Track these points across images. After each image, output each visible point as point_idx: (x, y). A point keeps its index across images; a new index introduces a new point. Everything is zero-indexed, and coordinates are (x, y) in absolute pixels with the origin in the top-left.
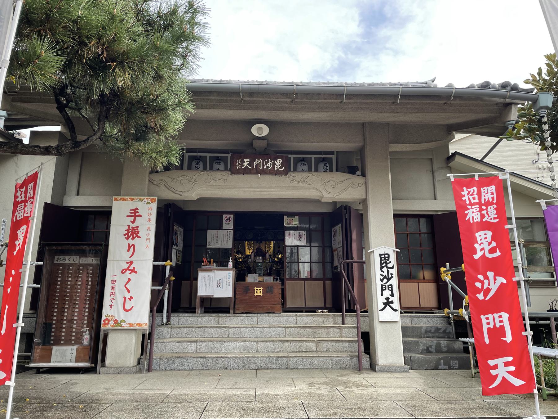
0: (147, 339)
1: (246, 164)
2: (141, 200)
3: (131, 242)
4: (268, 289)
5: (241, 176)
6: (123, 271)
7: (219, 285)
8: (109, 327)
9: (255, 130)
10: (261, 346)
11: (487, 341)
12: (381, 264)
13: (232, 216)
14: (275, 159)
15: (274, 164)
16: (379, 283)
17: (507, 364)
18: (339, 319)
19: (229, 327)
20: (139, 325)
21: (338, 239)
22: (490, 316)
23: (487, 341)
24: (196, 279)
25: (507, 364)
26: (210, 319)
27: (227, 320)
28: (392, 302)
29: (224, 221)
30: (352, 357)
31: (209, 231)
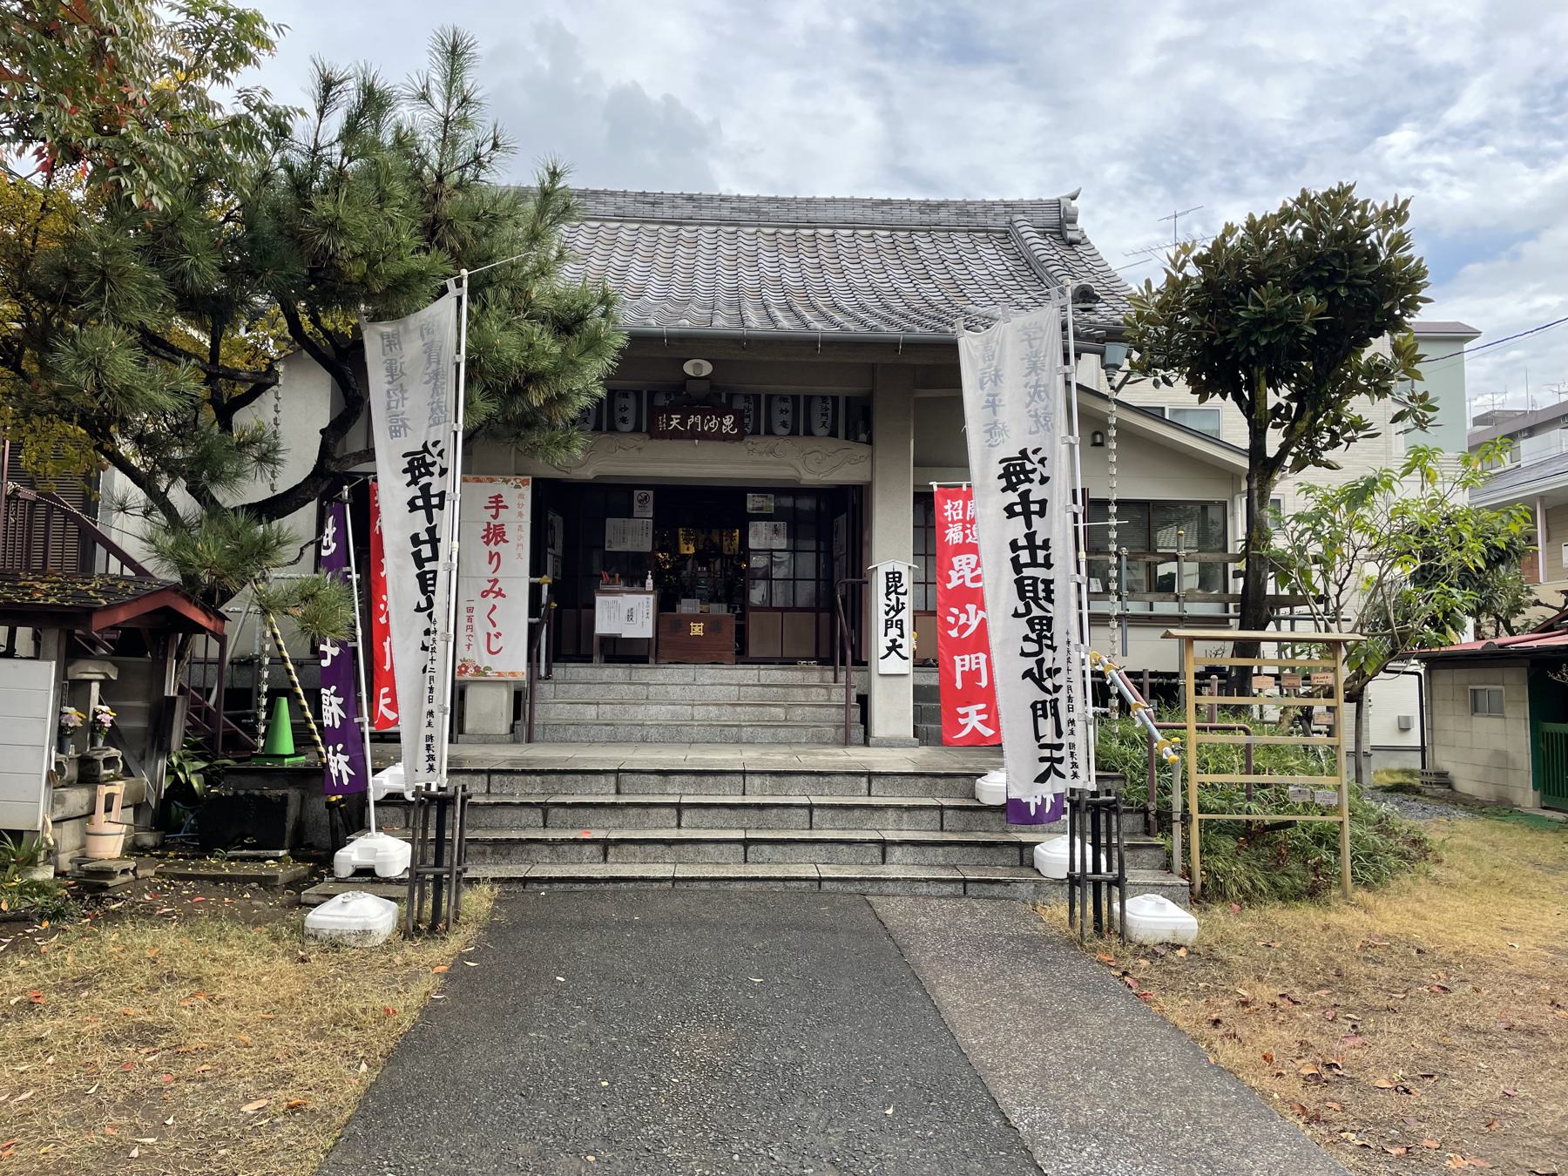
0: (521, 701)
1: (674, 423)
2: (506, 482)
3: (492, 548)
4: (713, 626)
5: (667, 441)
6: (484, 594)
7: (630, 617)
8: (467, 677)
9: (688, 368)
10: (700, 712)
11: (959, 685)
12: (888, 587)
13: (651, 493)
14: (722, 416)
15: (721, 423)
16: (882, 618)
17: (979, 712)
18: (830, 675)
19: (648, 684)
20: (513, 674)
21: (841, 539)
22: (967, 657)
23: (959, 685)
24: (593, 606)
25: (979, 712)
26: (618, 672)
27: (643, 673)
28: (900, 646)
29: (636, 503)
30: (838, 727)
31: (610, 522)
